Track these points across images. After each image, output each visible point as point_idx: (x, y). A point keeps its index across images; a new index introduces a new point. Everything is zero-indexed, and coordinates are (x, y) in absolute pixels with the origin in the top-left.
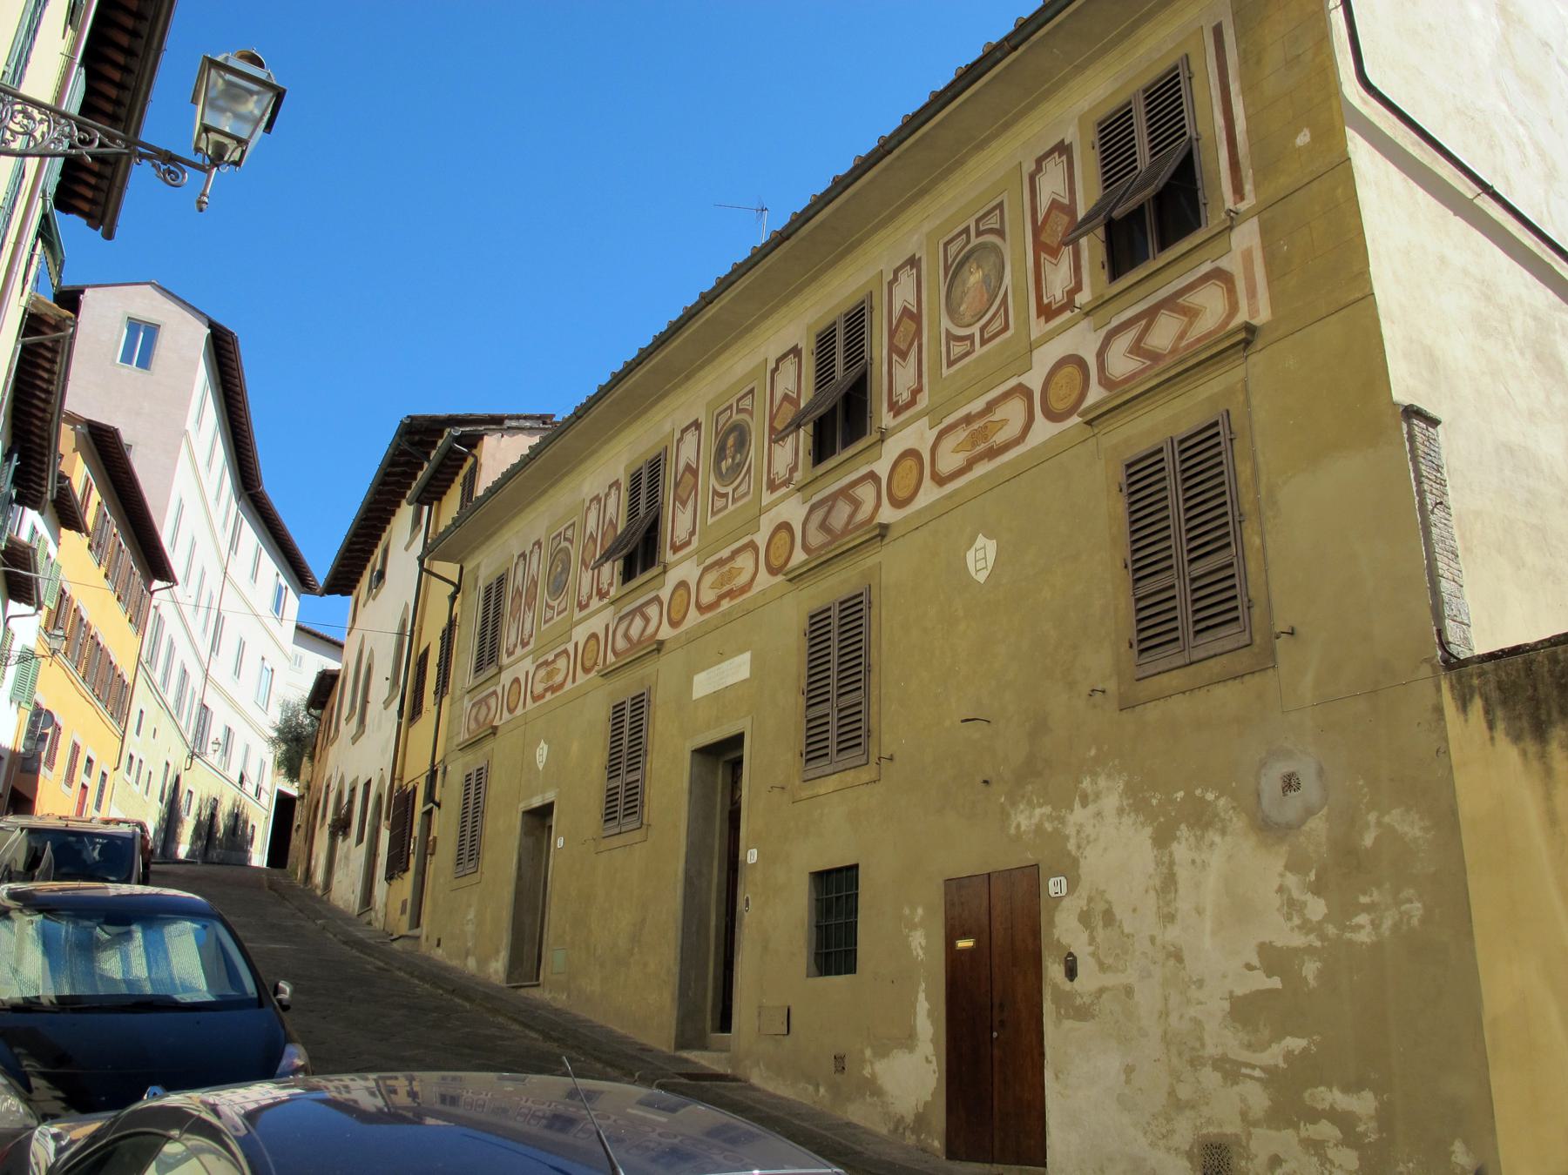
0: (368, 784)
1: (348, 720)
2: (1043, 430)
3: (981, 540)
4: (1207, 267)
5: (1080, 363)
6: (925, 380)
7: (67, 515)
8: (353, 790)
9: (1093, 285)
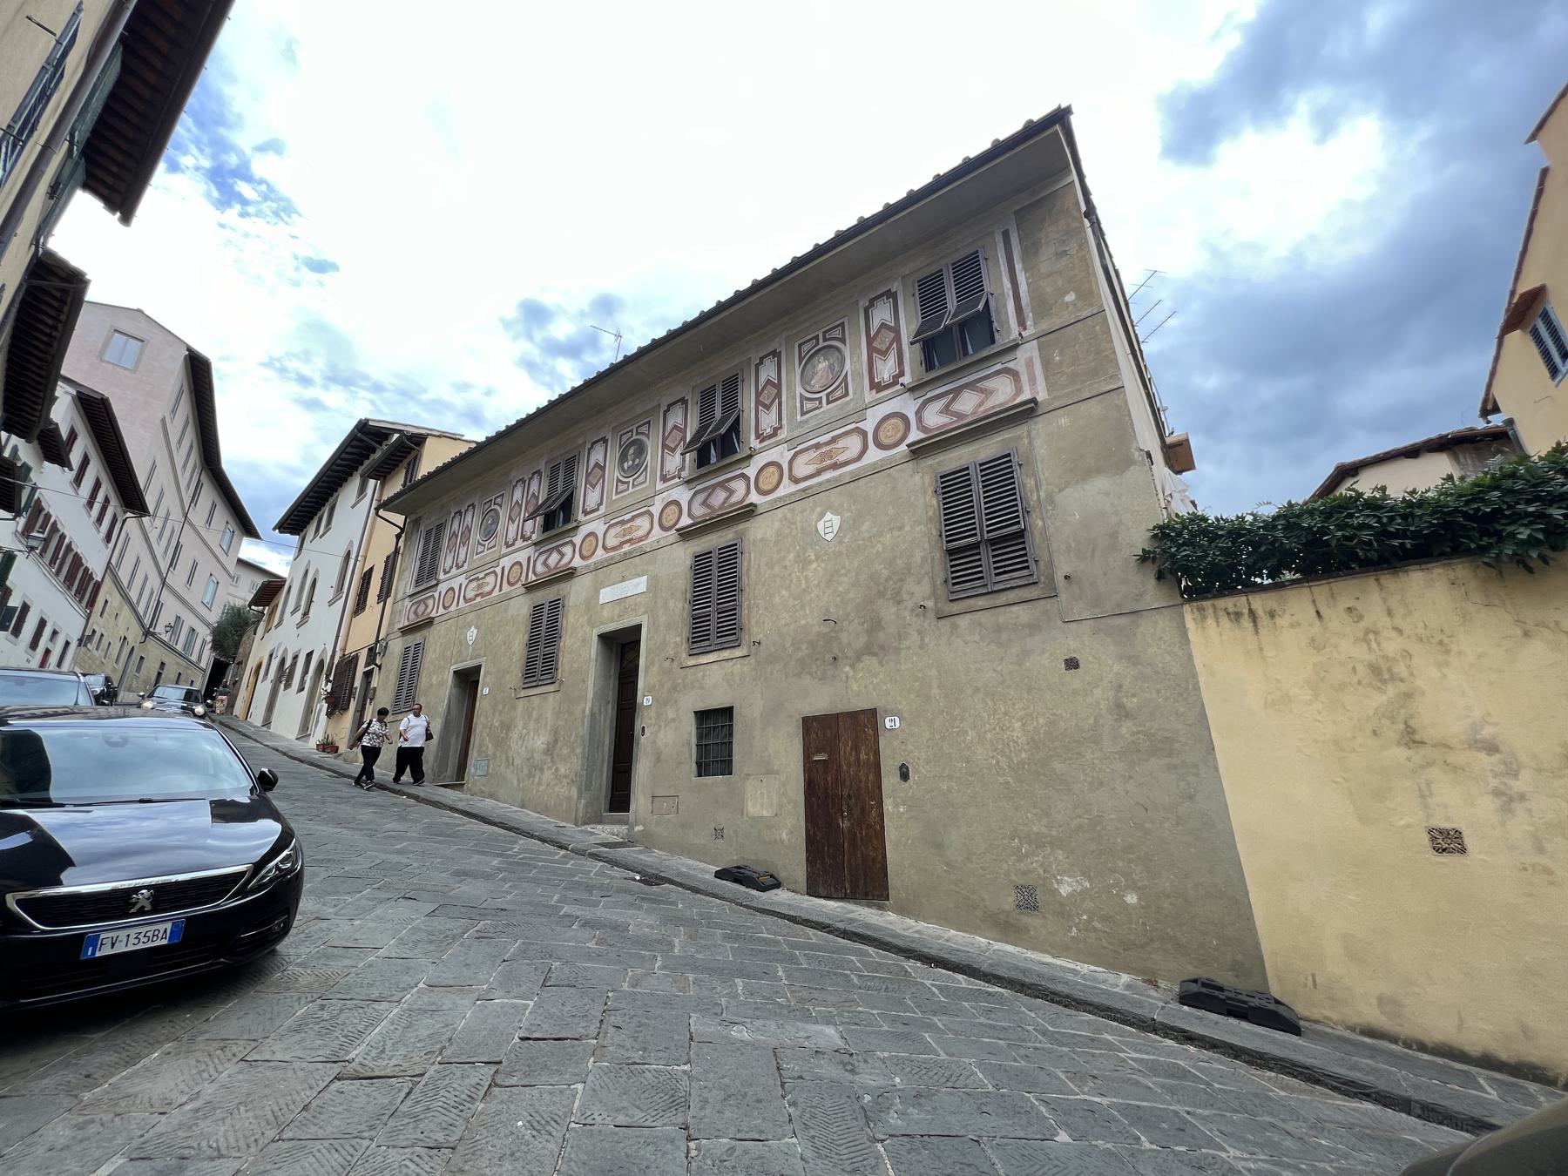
0: (310, 655)
1: (293, 613)
2: (874, 455)
3: (829, 516)
4: (999, 367)
5: (904, 418)
6: (784, 422)
7: (54, 450)
8: (295, 657)
9: (912, 373)
